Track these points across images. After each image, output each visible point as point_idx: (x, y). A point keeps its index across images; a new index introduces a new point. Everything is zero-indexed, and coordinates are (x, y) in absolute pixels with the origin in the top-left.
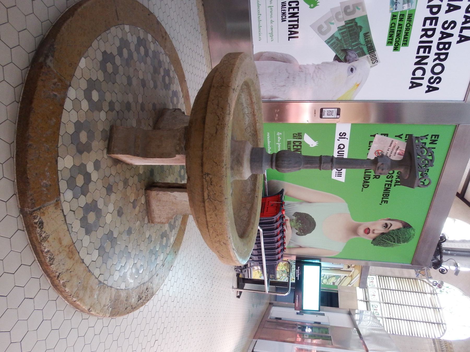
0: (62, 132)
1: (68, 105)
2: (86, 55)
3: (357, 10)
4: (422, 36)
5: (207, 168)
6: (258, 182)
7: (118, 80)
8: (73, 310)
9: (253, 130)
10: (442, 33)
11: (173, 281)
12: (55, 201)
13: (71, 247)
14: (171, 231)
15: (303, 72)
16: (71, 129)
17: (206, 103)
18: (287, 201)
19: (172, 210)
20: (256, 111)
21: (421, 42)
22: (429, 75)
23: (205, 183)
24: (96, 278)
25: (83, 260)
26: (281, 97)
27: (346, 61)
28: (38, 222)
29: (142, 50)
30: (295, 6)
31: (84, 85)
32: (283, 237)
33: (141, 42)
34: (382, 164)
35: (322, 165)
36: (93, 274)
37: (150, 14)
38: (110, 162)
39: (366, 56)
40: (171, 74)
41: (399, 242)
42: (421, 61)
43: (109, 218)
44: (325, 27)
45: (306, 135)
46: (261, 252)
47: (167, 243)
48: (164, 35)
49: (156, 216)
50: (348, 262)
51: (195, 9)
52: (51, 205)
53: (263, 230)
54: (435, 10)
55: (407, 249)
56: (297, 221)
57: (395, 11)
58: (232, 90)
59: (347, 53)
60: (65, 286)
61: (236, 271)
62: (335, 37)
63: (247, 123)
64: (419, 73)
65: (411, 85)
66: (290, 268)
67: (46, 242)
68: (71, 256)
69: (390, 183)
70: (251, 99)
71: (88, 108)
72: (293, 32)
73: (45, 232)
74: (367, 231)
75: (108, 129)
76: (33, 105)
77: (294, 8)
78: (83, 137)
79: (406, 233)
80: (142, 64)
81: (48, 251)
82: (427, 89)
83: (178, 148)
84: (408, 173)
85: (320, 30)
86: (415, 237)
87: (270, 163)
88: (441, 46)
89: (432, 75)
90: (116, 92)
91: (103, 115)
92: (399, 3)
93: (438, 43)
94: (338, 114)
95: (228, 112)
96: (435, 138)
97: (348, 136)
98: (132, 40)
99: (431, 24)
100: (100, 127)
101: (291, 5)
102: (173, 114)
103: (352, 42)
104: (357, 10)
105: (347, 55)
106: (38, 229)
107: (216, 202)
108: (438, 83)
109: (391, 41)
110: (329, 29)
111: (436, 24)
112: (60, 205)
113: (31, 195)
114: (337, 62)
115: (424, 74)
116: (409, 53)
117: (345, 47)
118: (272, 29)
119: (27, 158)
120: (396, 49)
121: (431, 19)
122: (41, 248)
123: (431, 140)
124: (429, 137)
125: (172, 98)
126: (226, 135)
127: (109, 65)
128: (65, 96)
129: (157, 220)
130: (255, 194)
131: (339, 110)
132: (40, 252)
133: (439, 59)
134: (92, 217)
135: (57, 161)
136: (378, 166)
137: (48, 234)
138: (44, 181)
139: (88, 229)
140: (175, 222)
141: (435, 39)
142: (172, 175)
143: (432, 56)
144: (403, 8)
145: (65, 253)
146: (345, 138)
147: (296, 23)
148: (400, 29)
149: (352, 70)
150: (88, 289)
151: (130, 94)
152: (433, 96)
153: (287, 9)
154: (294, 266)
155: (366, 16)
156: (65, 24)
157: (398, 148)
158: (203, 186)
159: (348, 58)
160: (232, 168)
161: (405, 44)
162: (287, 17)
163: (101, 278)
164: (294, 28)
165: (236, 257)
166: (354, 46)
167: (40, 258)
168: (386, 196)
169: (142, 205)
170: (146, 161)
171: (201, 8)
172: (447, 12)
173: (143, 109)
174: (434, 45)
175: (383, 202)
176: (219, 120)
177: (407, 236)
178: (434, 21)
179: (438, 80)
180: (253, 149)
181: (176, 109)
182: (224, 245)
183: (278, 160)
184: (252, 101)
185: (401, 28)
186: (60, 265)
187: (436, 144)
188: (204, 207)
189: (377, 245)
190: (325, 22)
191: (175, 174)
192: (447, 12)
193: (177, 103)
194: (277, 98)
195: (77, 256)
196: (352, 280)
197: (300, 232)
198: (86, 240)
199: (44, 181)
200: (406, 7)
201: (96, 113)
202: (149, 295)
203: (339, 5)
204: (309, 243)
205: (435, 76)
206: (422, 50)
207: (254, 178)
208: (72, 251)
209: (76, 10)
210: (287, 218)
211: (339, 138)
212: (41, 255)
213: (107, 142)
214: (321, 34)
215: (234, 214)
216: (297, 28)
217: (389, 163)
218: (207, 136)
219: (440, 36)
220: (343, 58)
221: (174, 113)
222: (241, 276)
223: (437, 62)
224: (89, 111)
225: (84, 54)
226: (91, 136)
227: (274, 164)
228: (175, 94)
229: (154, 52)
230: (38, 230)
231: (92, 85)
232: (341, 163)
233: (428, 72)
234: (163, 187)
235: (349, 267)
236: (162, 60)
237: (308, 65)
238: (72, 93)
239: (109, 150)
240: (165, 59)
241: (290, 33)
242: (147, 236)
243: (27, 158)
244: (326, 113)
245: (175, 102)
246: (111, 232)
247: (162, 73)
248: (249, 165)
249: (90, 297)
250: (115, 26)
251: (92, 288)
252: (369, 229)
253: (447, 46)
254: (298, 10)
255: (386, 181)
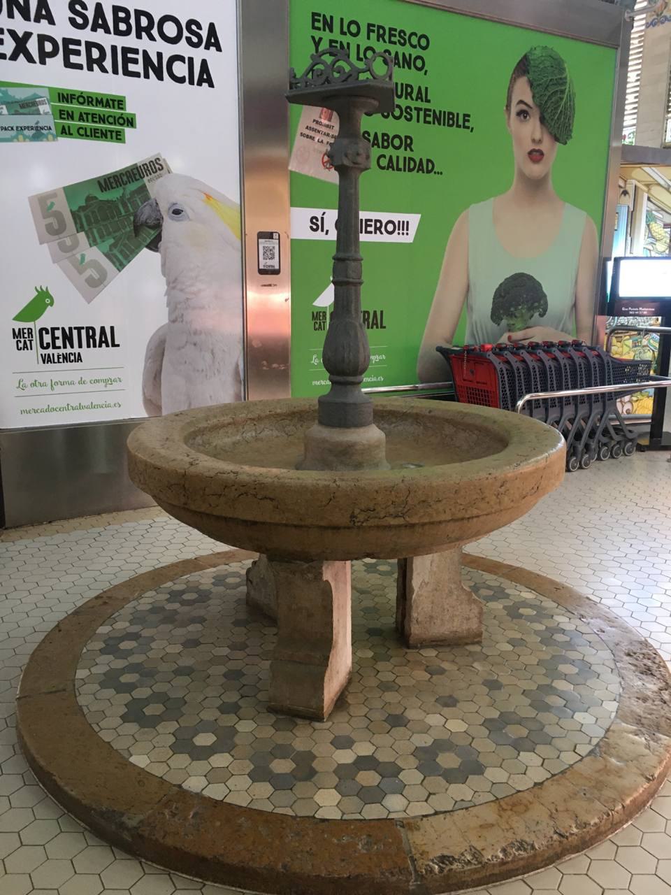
0: (268, 807)
1: (216, 792)
2: (125, 754)
3: (54, 208)
4: (104, 70)
5: (341, 519)
6: (399, 409)
7: (180, 695)
8: (647, 814)
9: (291, 420)
10: (94, 29)
11: (625, 598)
12: (402, 829)
13: (505, 807)
14: (507, 596)
15: (182, 315)
16: (265, 789)
17: (218, 518)
18: (465, 339)
19: (451, 592)
20: (250, 416)
21: (115, 71)
22: (182, 48)
23: (372, 522)
24: (581, 760)
25: (536, 784)
26: (235, 356)
27: (158, 226)
28: (439, 866)
29: (126, 645)
30: (50, 335)
31: (182, 760)
32: (548, 346)
33: (111, 647)
34: (346, 156)
35: (351, 280)
36: (571, 766)
37: (58, 628)
38: (341, 718)
39: (147, 184)
40: (178, 587)
41: (562, 82)
42: (155, 68)
43: (456, 726)
44: (90, 272)
45: (314, 304)
46: (596, 395)
47: (531, 606)
48: (100, 602)
49: (465, 627)
50: (612, 194)
51: (58, 538)
52: (410, 836)
53: (529, 392)
54: (48, 47)
55: (578, 59)
56: (512, 315)
57: (53, 131)
58: (192, 469)
59: (142, 225)
60: (585, 823)
61: (630, 452)
62: (111, 250)
63: (275, 433)
64: (180, 69)
65: (205, 85)
66: (626, 329)
67: (483, 852)
68: (522, 808)
69: (422, 113)
70: (223, 426)
71: (227, 754)
72: (103, 338)
73: (462, 854)
74: (536, 156)
75: (273, 718)
76: (209, 857)
77: (54, 338)
78: (282, 766)
79: (541, 66)
80: (153, 645)
81: (504, 850)
82: (213, 49)
83: (310, 576)
84: (363, 100)
85: (96, 283)
86: (550, 46)
87: (349, 387)
88: (123, 27)
89: (184, 40)
90: (202, 697)
91: (245, 727)
92: (37, 123)
93: (115, 34)
94: (270, 236)
95: (232, 475)
96: (319, 21)
97: (317, 213)
98: (105, 664)
99: (78, 53)
100: (268, 732)
101: (48, 344)
102: (257, 584)
103: (119, 216)
104: (54, 208)
105: (145, 224)
106: (454, 867)
107: (410, 502)
108: (199, 27)
109: (114, 134)
110: (95, 265)
111: (78, 43)
112: (412, 821)
113: (383, 873)
114: (161, 245)
115: (181, 59)
116: (138, 93)
117: (130, 229)
118: (97, 381)
119: (309, 876)
120: (130, 122)
121: (68, 53)
122: (494, 865)
123: (324, 30)
124: (318, 34)
125: (228, 586)
126: (276, 480)
127: (148, 711)
128: (199, 796)
129: (474, 625)
130: (423, 416)
131: (262, 235)
132: (504, 868)
133: (148, 30)
134: (448, 760)
135: (324, 820)
136: (352, 165)
137: (468, 849)
138: (360, 847)
139: (473, 768)
140: (489, 588)
141: (107, 40)
142: (386, 590)
143: (143, 44)
144: (46, 114)
145: (515, 818)
146: (322, 218)
147: (83, 332)
148: (90, 117)
149: (177, 212)
150: (601, 778)
151: (210, 672)
152: (228, 36)
153: (56, 352)
154: (623, 320)
155: (65, 188)
156: (66, 788)
157: (317, 122)
158: (378, 527)
159: (151, 222)
160: (358, 466)
161: (119, 102)
162: (72, 351)
163: (583, 750)
164: (93, 337)
165: (537, 462)
166: (127, 211)
167: (517, 870)
168: (453, 119)
169: (441, 655)
170: (340, 641)
171: (56, 525)
172: (52, 22)
173: (243, 647)
174: (121, 42)
175: (467, 124)
176: (246, 493)
177: (548, 64)
178: (71, 47)
179: (194, 27)
180: (321, 423)
181: (248, 579)
182: (508, 485)
183: (344, 368)
184: (229, 424)
185: (87, 114)
186: (537, 830)
187: (332, 18)
188: (423, 525)
189: (571, 131)
190: (80, 272)
191: (385, 585)
192: (52, 22)
193: (239, 576)
194: (237, 366)
195: (525, 794)
196: (659, 184)
197: (537, 308)
198: (494, 774)
199: (360, 847)
200: (45, 108)
201: (237, 740)
202: (644, 651)
203: (45, 245)
204: (561, 287)
205: (186, 34)
206: (132, 67)
207: (383, 416)
208: (510, 804)
209: (41, 768)
210: (504, 340)
211: (322, 230)
212: (511, 866)
213: (299, 721)
214: (105, 279)
215: (461, 461)
216: (93, 329)
217: (345, 141)
218: (277, 518)
219: (100, 31)
220: (153, 233)
221: (254, 583)
222: (645, 442)
223: (155, 32)
224: (232, 753)
225: (123, 757)
226: (282, 751)
227: (351, 379)
228: (219, 580)
229: (131, 622)
230: (455, 866)
231: (183, 744)
232: (348, 226)
233: (174, 50)
234: (404, 609)
235: (625, 193)
236: (149, 607)
237: (168, 305)
238: (195, 784)
239: (315, 716)
240: (149, 599)
241: (104, 345)
242: (510, 648)
243: (309, 876)
244: (269, 262)
245: (238, 580)
246: (488, 723)
247: (176, 606)
248: (353, 430)
249: (620, 777)
250: (76, 697)
251: (600, 770)
252: (530, 153)
253: (122, 15)
254: (58, 329)
255: (418, 121)
